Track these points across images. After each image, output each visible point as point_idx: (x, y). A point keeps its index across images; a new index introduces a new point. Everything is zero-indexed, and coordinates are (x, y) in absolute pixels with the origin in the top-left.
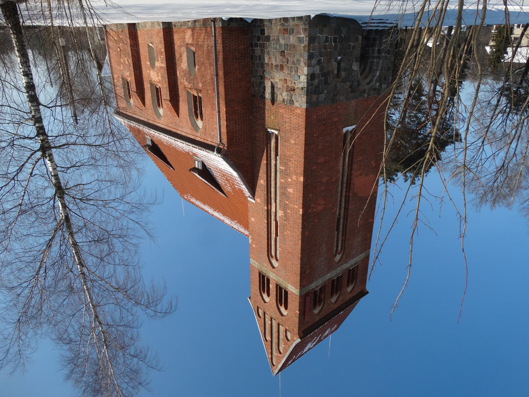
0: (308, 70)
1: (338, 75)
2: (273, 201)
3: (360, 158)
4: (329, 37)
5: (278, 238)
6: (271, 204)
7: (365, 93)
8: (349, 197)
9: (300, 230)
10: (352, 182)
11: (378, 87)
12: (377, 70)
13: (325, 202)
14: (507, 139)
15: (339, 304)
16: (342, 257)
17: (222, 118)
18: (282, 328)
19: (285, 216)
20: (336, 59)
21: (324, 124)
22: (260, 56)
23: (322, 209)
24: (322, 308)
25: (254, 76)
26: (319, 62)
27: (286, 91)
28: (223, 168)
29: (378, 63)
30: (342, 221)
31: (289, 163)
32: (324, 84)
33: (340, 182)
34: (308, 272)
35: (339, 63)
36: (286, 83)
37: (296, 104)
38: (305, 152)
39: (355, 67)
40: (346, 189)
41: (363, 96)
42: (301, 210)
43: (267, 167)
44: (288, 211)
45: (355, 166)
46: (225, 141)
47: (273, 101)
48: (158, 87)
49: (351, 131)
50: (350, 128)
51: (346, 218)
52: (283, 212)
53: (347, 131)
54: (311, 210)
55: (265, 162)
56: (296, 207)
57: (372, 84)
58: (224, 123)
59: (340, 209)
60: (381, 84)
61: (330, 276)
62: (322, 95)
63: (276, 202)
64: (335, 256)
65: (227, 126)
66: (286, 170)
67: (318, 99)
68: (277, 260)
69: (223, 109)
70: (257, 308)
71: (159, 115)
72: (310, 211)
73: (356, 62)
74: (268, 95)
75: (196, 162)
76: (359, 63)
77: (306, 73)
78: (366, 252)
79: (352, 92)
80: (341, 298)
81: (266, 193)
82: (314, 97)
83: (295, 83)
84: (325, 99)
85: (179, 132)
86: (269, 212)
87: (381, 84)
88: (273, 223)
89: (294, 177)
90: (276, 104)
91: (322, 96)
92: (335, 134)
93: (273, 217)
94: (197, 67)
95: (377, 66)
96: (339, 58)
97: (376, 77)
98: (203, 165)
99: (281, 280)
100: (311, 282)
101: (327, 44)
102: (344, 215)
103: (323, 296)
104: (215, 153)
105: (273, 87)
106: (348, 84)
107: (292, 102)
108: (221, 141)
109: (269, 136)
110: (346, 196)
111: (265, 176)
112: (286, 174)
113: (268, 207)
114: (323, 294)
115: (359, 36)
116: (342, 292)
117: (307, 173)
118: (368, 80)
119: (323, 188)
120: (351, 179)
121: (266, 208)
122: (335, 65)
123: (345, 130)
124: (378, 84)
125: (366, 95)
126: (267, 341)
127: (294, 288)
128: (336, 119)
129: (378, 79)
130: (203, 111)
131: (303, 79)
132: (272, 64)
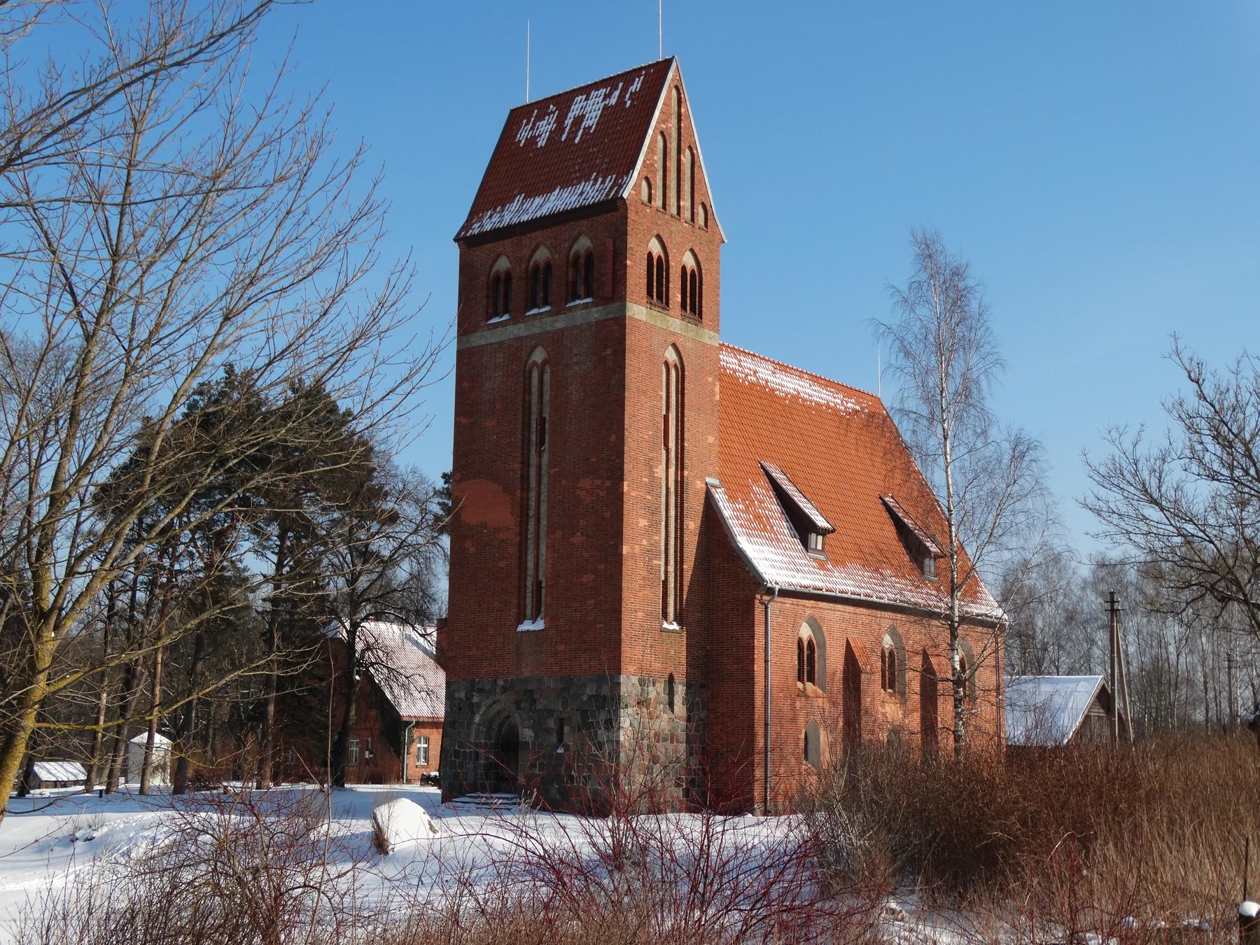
0: (618, 736)
1: (561, 722)
2: (672, 490)
3: (501, 564)
5: (664, 413)
6: (676, 482)
7: (503, 687)
8: (522, 489)
9: (626, 449)
10: (518, 519)
12: (479, 724)
16: (529, 355)
17: (762, 652)
18: (658, 202)
19: (651, 468)
20: (567, 748)
21: (585, 642)
23: (581, 480)
24: (571, 246)
25: (701, 720)
26: (600, 746)
28: (766, 548)
29: (477, 736)
30: (533, 437)
32: (587, 711)
33: (544, 522)
34: (609, 351)
35: (560, 740)
37: (635, 679)
38: (620, 599)
39: (527, 734)
40: (528, 505)
41: (505, 681)
42: (626, 489)
43: (682, 556)
44: (646, 480)
45: (513, 550)
46: (759, 610)
47: (671, 680)
48: (890, 691)
49: (525, 618)
50: (527, 626)
51: (526, 442)
52: (656, 475)
53: (534, 620)
55: (685, 567)
56: (633, 494)
57: (489, 701)
58: (759, 642)
59: (539, 466)
60: (469, 698)
61: (557, 321)
62: (590, 694)
63: (667, 488)
64: (545, 362)
65: (753, 637)
66: (650, 559)
67: (599, 688)
68: (666, 363)
69: (758, 667)
70: (709, 224)
71: (893, 633)
72: (608, 483)
73: (527, 743)
74: (680, 690)
75: (819, 547)
77: (622, 732)
78: (469, 346)
79: (531, 692)
80: (527, 251)
81: (685, 505)
82: (605, 690)
84: (584, 685)
85: (851, 609)
86: (681, 466)
87: (469, 698)
88: (672, 444)
90: (667, 676)
91: (590, 690)
92: (562, 621)
93: (673, 455)
94: (803, 736)
95: (477, 730)
96: (560, 751)
97: (481, 712)
98: (805, 543)
102: (529, 450)
103: (570, 274)
104: (777, 587)
105: (671, 704)
106: (539, 707)
107: (642, 683)
108: (766, 608)
109: (679, 619)
110: (528, 490)
111: (686, 539)
112: (651, 552)
113: (682, 476)
114: (570, 279)
116: (523, 266)
117: (616, 561)
118: (496, 708)
119: (582, 523)
120: (521, 526)
121: (686, 473)
122: (568, 739)
123: (540, 625)
124: (475, 699)
125: (500, 682)
126: (690, 148)
128: (561, 647)
129: (475, 709)
130: (796, 658)
131: (625, 722)
132: (672, 742)
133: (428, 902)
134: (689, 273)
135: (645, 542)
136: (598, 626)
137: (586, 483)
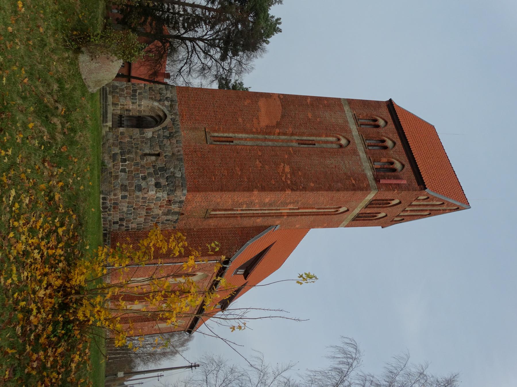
4: (121, 168)
11: (170, 103)
13: (282, 163)
14: (184, 269)
15: (397, 138)
22: (137, 224)
27: (171, 205)
31: (240, 202)
34: (354, 182)
36: (163, 206)
37: (183, 198)
54: (288, 181)
63: (280, 209)
76: (146, 129)
83: (163, 200)
89: (254, 198)
99: (361, 204)
100: (365, 176)
101: (127, 170)
115: (120, 131)
116: (384, 134)
124: (166, 103)
127: (369, 195)
132: (145, 216)
133: (139, 242)
134: (376, 215)
135: (257, 201)
136: (213, 177)
137: (287, 169)
